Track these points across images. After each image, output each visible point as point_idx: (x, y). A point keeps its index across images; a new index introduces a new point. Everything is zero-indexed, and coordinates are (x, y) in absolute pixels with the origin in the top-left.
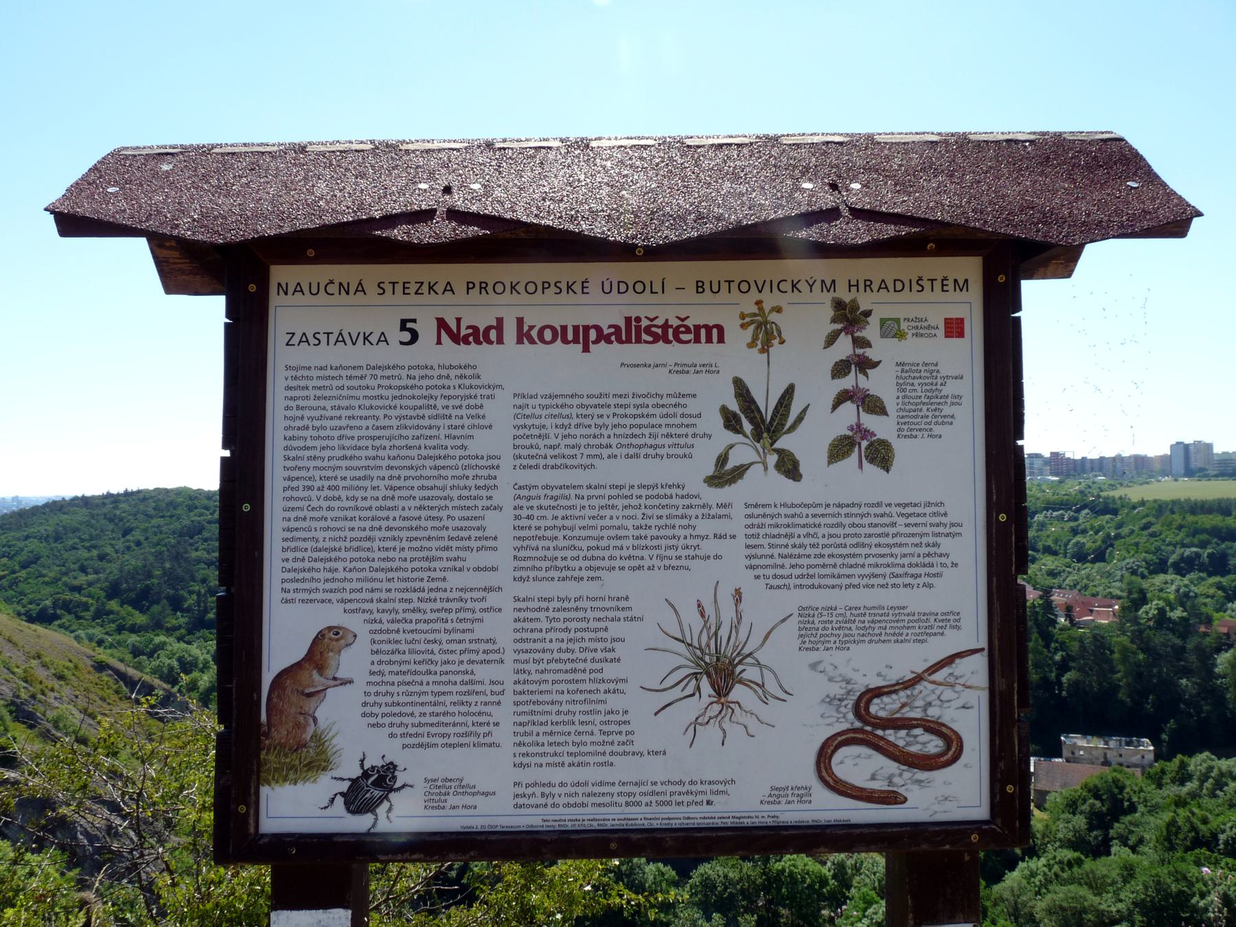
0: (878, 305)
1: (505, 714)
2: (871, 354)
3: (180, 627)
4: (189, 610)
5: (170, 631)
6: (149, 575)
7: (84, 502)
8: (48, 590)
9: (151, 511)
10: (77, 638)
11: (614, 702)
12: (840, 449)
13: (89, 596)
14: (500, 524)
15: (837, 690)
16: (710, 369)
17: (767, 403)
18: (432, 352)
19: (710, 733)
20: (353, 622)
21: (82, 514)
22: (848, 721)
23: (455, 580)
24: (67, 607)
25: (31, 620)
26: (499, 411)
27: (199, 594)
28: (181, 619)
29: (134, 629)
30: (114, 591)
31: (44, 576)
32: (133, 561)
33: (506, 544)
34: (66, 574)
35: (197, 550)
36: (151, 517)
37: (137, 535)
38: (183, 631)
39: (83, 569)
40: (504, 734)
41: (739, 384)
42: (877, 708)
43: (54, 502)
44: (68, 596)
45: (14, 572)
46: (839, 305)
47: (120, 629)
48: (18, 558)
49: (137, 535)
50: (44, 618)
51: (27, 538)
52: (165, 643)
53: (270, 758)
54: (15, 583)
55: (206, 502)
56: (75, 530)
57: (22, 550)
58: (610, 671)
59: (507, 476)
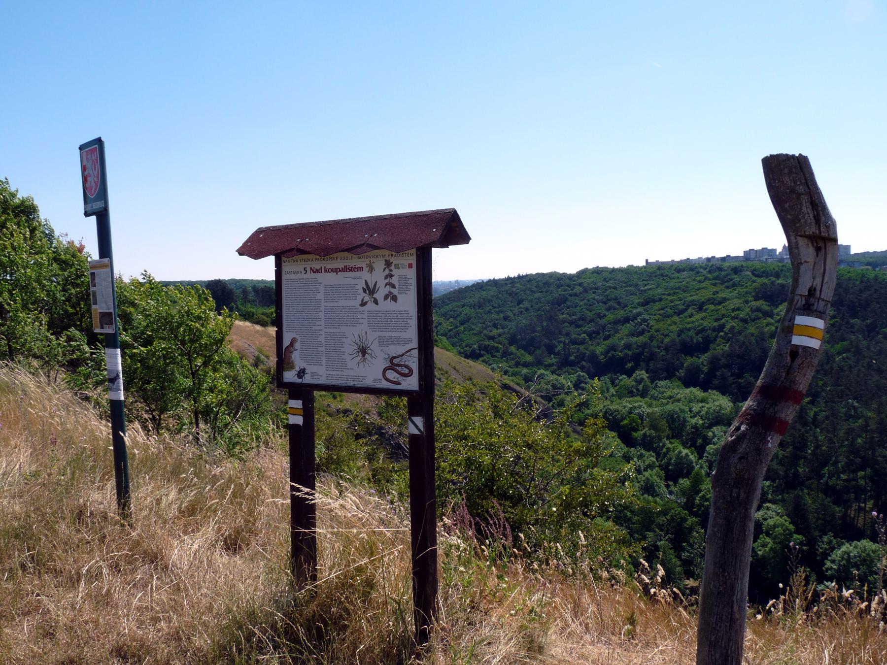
0: (394, 260)
1: (324, 358)
2: (393, 273)
3: (553, 364)
4: (558, 354)
5: (547, 367)
6: (534, 331)
7: (494, 283)
8: (476, 338)
9: (534, 289)
10: (493, 369)
11: (343, 357)
12: (386, 297)
13: (499, 343)
14: (322, 315)
15: (386, 356)
16: (360, 278)
17: (371, 286)
18: (310, 275)
19: (361, 365)
20: (297, 337)
21: (493, 291)
22: (389, 364)
23: (314, 328)
24: (487, 349)
25: (467, 357)
26: (321, 289)
27: (564, 343)
28: (554, 360)
29: (526, 365)
30: (513, 341)
31: (473, 330)
32: (524, 321)
33: (323, 320)
34: (486, 328)
35: (563, 314)
36: (534, 292)
37: (526, 304)
38: (555, 367)
39: (495, 326)
40: (324, 363)
41: (366, 281)
42: (395, 361)
43: (478, 283)
44: (487, 343)
45: (456, 327)
46: (386, 261)
47: (517, 364)
48: (459, 319)
49: (526, 304)
50: (473, 355)
51: (463, 306)
52: (543, 374)
53: (285, 366)
54: (458, 333)
55: (568, 282)
56: (490, 301)
57: (461, 313)
58: (342, 350)
59: (323, 304)
